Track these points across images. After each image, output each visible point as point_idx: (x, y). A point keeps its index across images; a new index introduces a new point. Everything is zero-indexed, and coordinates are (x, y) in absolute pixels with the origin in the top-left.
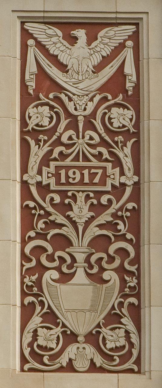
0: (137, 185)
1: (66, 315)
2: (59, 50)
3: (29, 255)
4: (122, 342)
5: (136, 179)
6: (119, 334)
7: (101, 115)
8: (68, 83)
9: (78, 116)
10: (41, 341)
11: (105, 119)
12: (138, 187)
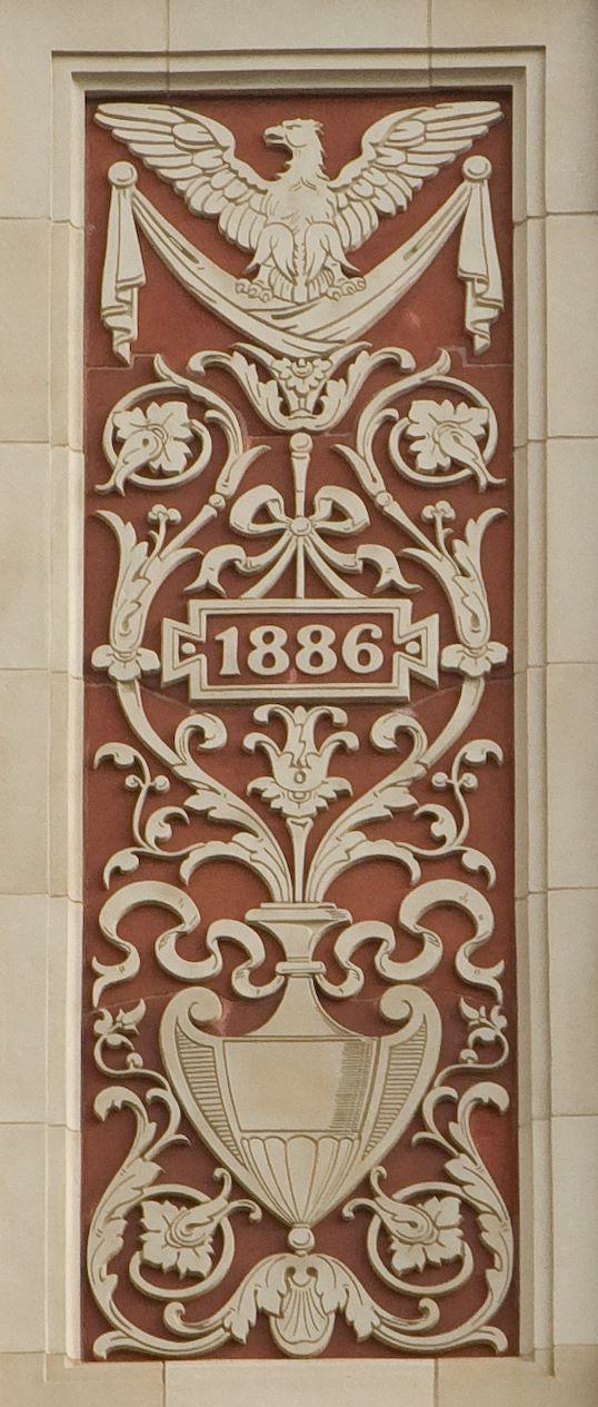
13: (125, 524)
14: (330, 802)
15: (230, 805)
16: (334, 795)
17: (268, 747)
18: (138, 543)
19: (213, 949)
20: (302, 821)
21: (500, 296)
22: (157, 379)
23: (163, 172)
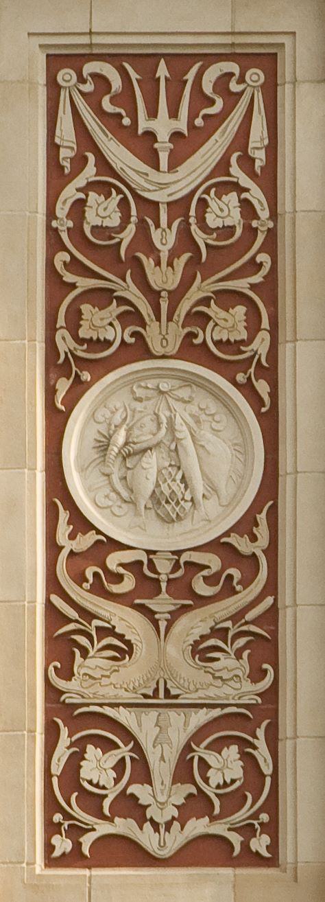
1: (218, 152)
2: (211, 422)
3: (216, 98)
5: (271, 225)
7: (64, 82)
11: (55, 537)
13: (96, 749)
14: (98, 339)
15: (95, 756)
20: (263, 532)
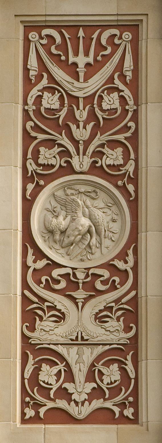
0: (136, 112)
4: (117, 104)
5: (135, 108)
6: (114, 97)
8: (66, 308)
9: (79, 141)
10: (45, 104)
12: (136, 223)
16: (131, 135)
17: (133, 329)
18: (77, 129)
19: (60, 279)
21: (32, 69)
22: (114, 84)
23: (68, 91)
